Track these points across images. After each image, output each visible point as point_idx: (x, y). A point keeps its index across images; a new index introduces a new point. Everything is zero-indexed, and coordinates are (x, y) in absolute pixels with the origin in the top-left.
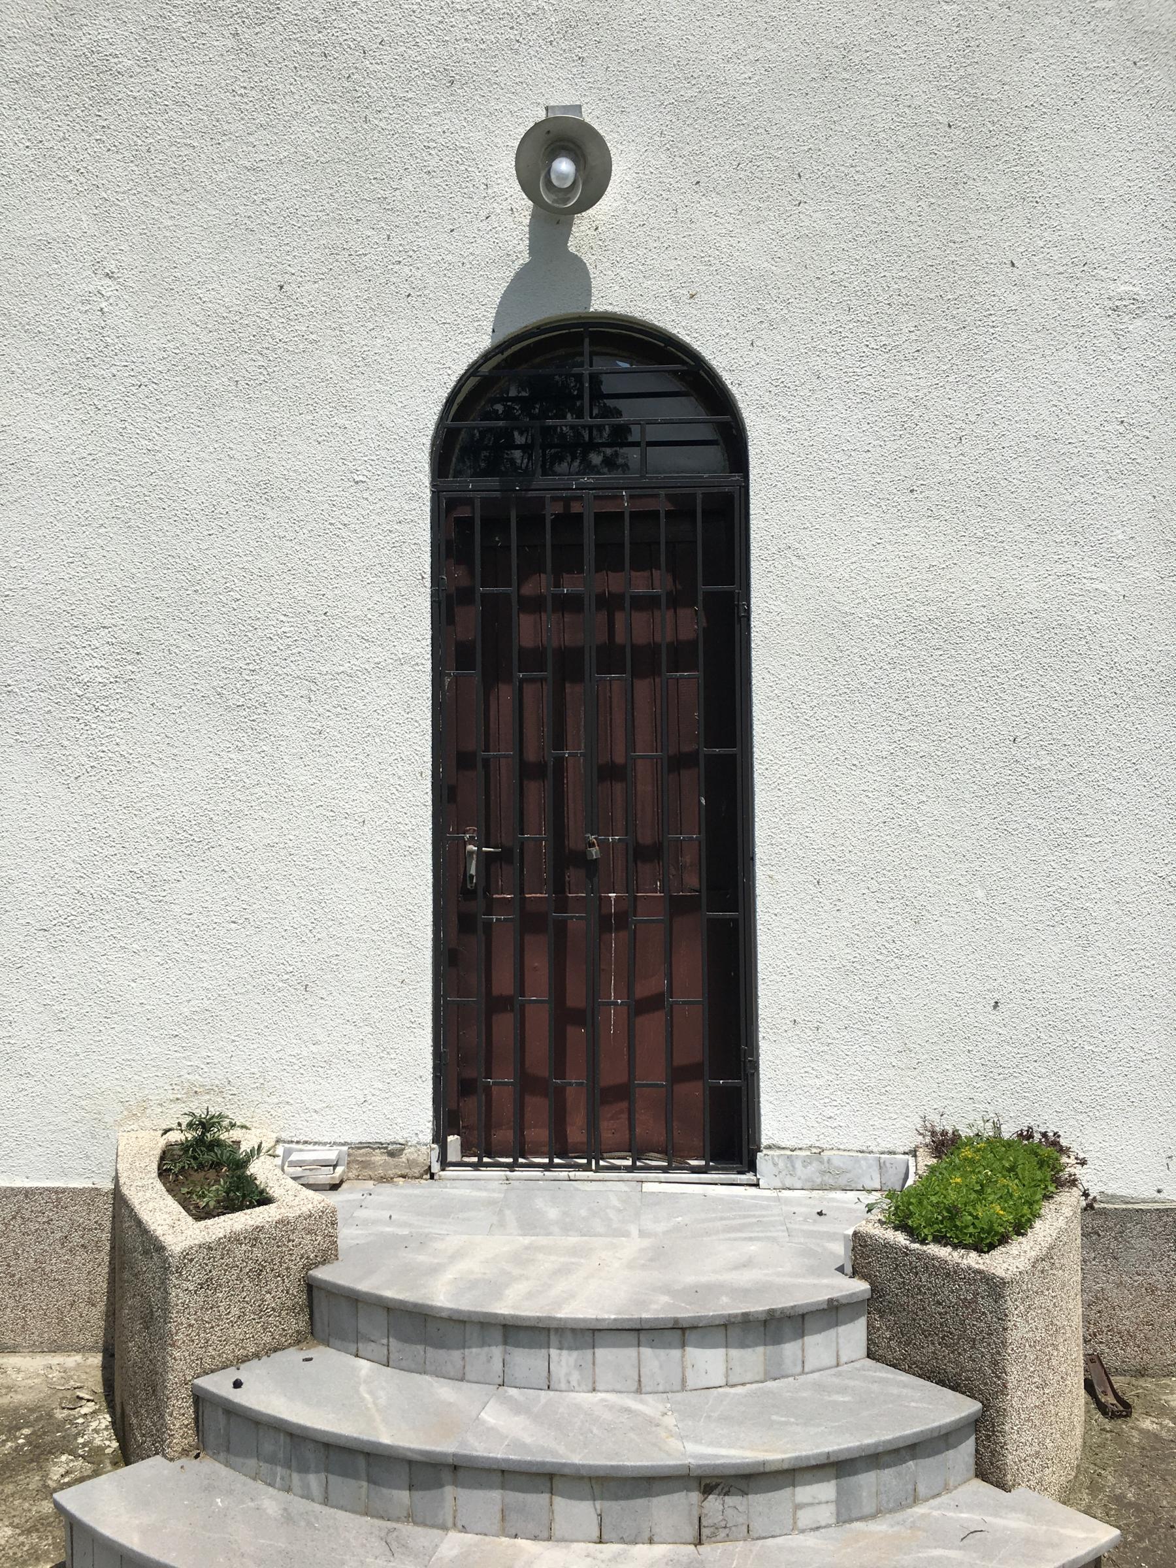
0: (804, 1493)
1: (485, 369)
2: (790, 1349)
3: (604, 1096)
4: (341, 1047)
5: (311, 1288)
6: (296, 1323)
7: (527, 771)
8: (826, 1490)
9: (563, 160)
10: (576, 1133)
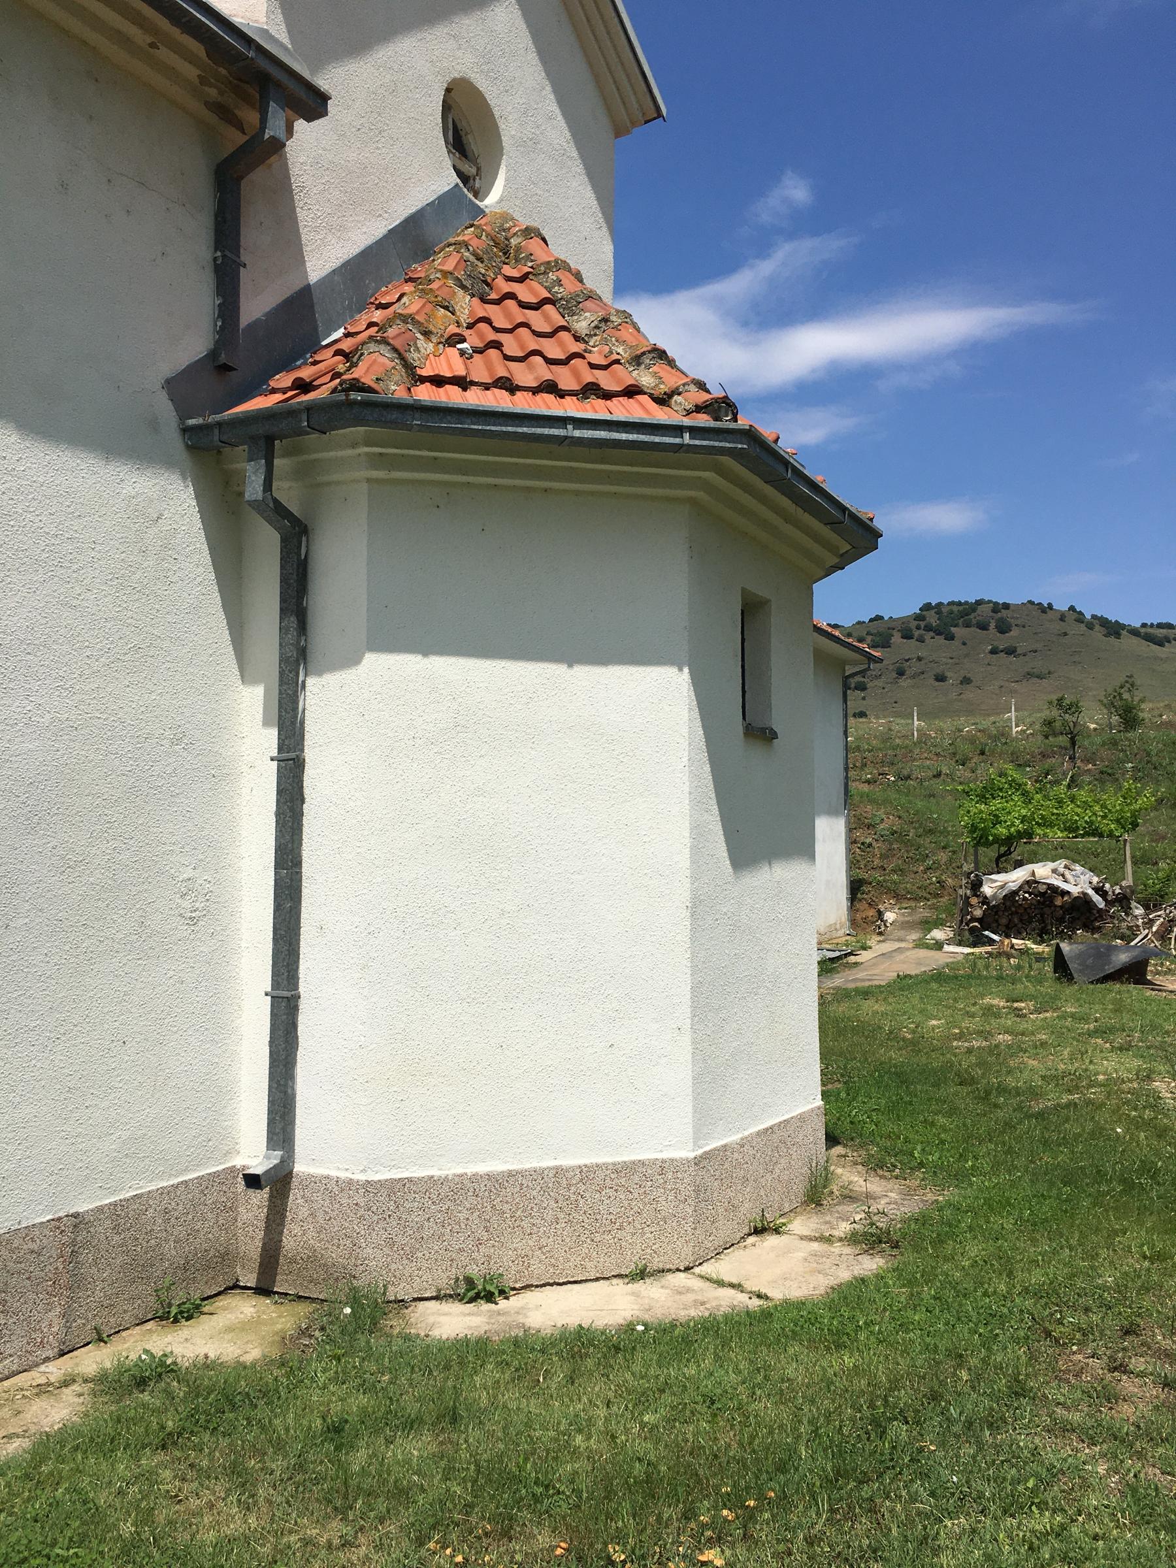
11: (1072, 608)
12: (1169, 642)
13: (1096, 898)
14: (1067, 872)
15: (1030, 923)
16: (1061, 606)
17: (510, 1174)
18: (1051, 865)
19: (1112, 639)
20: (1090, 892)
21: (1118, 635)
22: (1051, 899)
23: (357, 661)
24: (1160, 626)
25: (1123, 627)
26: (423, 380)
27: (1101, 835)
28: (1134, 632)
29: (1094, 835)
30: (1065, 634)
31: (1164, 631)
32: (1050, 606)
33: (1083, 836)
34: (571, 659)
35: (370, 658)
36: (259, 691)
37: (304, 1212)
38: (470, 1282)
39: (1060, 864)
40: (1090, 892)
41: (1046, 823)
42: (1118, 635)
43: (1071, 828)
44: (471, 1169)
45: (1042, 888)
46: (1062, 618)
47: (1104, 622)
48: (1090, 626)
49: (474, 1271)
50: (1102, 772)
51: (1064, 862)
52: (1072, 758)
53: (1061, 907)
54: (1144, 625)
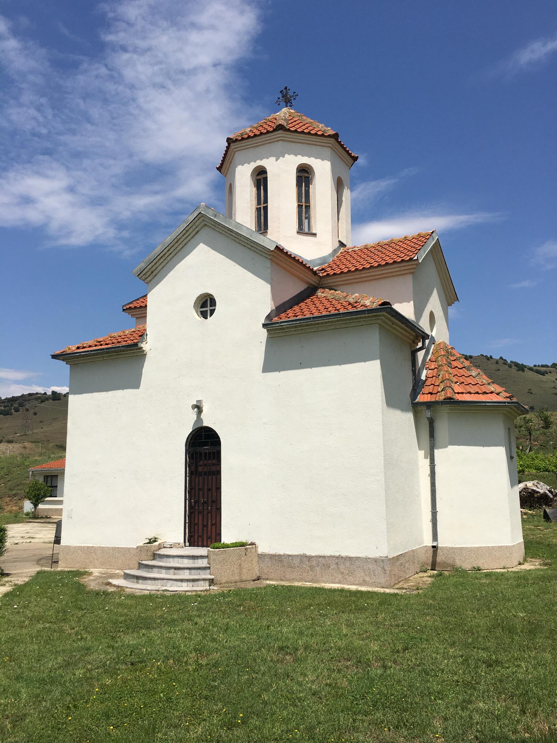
0: (185, 571)
1: (193, 433)
2: (196, 561)
3: (208, 538)
4: (172, 528)
5: (154, 554)
6: (152, 558)
7: (200, 489)
8: (188, 571)
9: (198, 408)
10: (205, 544)
11: (501, 358)
12: (547, 373)
13: (550, 494)
14: (538, 485)
15: (526, 503)
16: (496, 357)
17: (480, 547)
18: (532, 482)
19: (520, 372)
20: (547, 492)
21: (523, 370)
22: (533, 495)
23: (447, 447)
24: (542, 366)
25: (525, 366)
26: (456, 393)
27: (549, 471)
28: (531, 369)
29: (546, 471)
30: (499, 370)
31: (545, 369)
32: (491, 357)
33: (542, 472)
34: (484, 445)
35: (449, 446)
36: (423, 452)
37: (442, 554)
38: (474, 568)
39: (535, 482)
40: (547, 492)
41: (528, 467)
42: (523, 370)
43: (538, 469)
44: (473, 546)
45: (530, 491)
46: (497, 362)
47: (516, 364)
48: (510, 366)
49: (475, 566)
50: (541, 445)
51: (536, 481)
52: (530, 440)
53: (537, 497)
54: (535, 366)
